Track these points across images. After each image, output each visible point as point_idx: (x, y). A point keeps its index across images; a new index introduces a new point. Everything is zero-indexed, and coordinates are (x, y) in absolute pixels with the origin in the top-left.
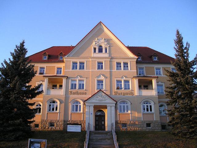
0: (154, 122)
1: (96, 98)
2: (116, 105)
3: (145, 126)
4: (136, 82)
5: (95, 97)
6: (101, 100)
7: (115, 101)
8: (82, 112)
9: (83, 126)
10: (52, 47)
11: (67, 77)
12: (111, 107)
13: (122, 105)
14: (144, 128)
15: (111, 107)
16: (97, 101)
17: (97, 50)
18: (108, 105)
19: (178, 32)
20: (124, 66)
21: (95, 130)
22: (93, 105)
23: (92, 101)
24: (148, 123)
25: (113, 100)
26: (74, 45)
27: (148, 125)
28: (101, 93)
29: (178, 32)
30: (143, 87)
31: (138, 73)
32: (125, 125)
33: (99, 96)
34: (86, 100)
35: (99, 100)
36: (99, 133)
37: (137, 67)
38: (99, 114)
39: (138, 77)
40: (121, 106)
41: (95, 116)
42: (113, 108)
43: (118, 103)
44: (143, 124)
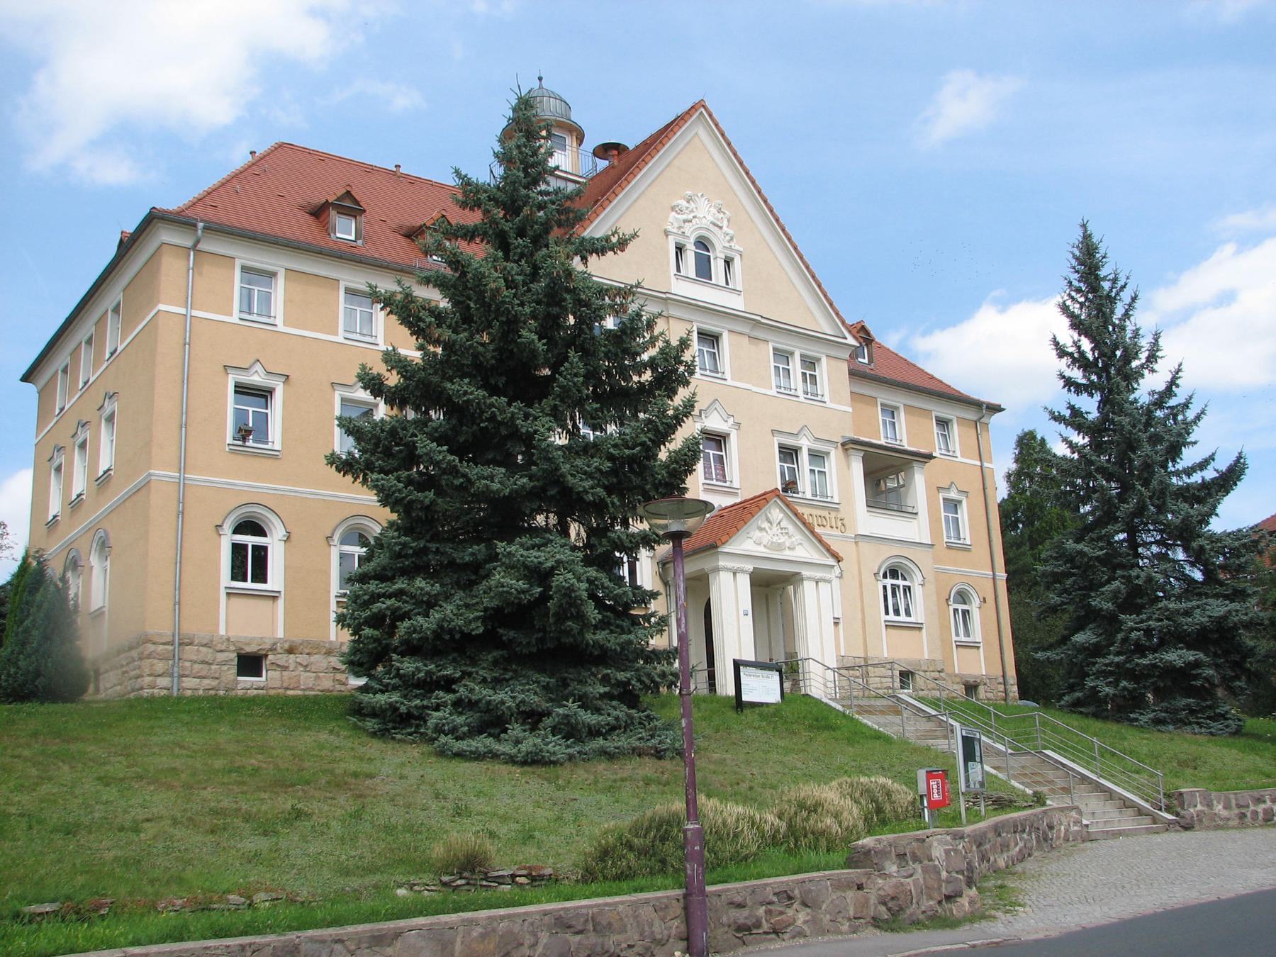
6: (779, 547)
16: (761, 551)
18: (806, 573)
25: (828, 549)
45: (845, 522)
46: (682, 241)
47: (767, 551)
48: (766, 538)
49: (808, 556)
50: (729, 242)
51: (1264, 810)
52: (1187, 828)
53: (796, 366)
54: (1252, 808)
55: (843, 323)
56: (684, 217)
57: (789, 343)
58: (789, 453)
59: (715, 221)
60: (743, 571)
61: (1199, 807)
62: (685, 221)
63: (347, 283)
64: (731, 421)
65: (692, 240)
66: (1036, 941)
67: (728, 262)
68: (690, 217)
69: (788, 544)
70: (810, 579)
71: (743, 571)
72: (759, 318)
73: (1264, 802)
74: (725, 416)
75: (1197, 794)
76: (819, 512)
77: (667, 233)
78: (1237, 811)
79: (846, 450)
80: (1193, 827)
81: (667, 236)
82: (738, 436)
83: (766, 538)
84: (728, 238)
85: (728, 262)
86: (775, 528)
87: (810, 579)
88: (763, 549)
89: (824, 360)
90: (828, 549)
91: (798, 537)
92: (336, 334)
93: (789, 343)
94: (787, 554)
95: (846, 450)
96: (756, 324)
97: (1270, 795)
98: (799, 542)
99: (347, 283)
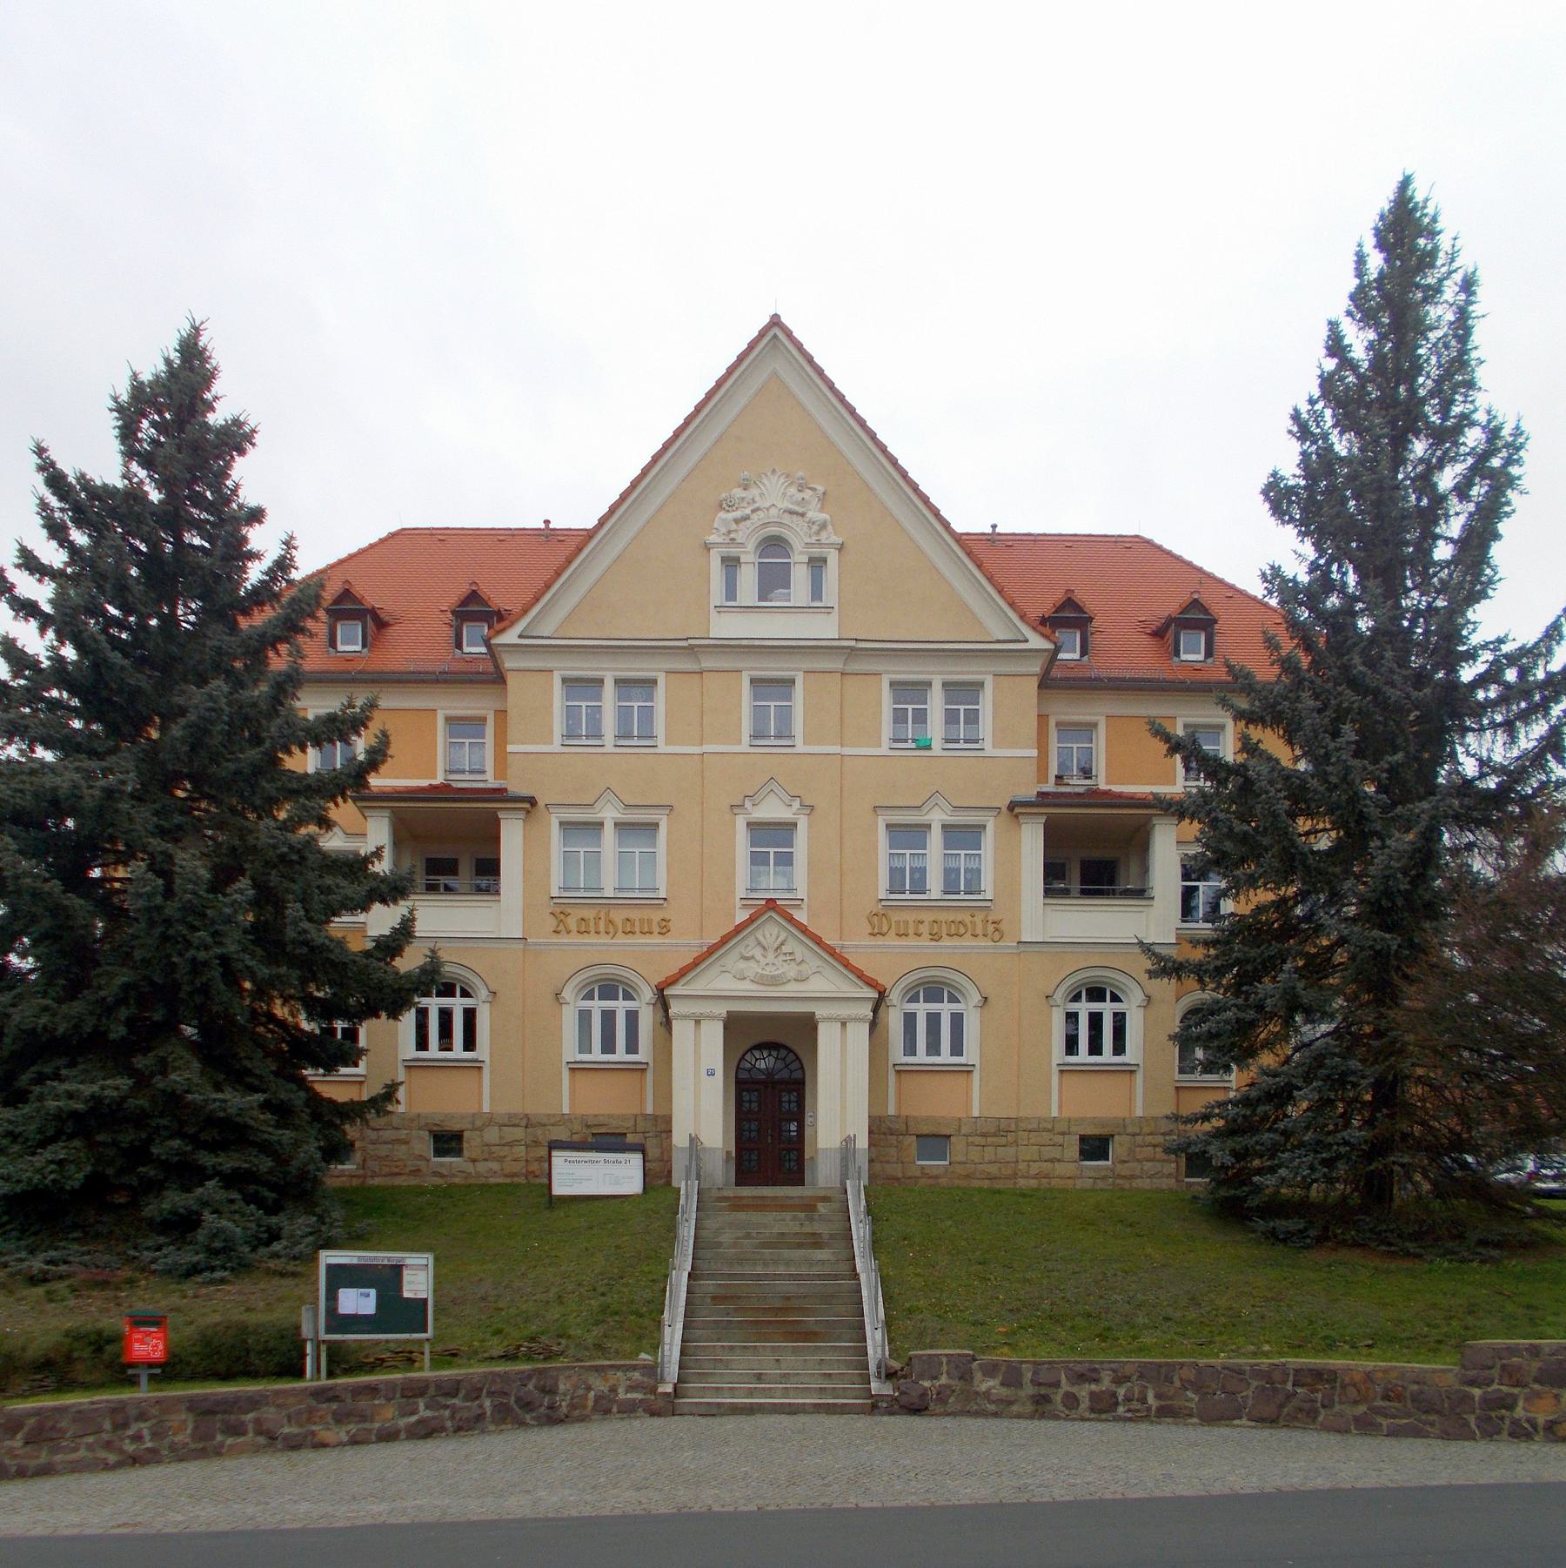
0: (1129, 1130)
1: (742, 965)
2: (875, 1011)
3: (1073, 1151)
4: (1031, 843)
5: (731, 960)
6: (775, 981)
7: (871, 983)
8: (643, 1055)
9: (653, 1152)
10: (393, 536)
11: (532, 801)
12: (844, 1024)
13: (922, 1009)
14: (1060, 1169)
15: (844, 1024)
16: (746, 987)
17: (748, 579)
18: (820, 1011)
19: (40, 451)
20: (951, 718)
21: (740, 1181)
22: (722, 1009)
23: (718, 986)
24: (1090, 1131)
25: (860, 975)
26: (580, 515)
27: (1095, 1147)
28: (771, 931)
29: (40, 451)
30: (1075, 873)
31: (1054, 771)
32: (934, 1141)
33: (758, 952)
34: (673, 981)
35: (760, 980)
36: (759, 1205)
37: (1042, 719)
38: (764, 1062)
39: (1044, 798)
40: (910, 1019)
41: (739, 1082)
42: (859, 1035)
43: (894, 996)
44: (1059, 1139)
45: (1002, 926)
46: (733, 551)
47: (762, 988)
48: (752, 969)
49: (833, 988)
50: (818, 533)
51: (1092, 1394)
52: (917, 1410)
53: (936, 704)
54: (1066, 1387)
55: (1022, 617)
56: (738, 514)
57: (974, 669)
58: (908, 835)
59: (791, 506)
60: (711, 1018)
61: (944, 1380)
62: (737, 521)
63: (752, 673)
64: (796, 804)
65: (751, 547)
66: (909, 1510)
67: (817, 564)
68: (748, 511)
69: (792, 974)
70: (829, 1019)
71: (711, 1018)
72: (853, 643)
73: (1097, 1381)
74: (787, 799)
75: (944, 1360)
76: (951, 916)
77: (707, 547)
78: (1029, 1390)
79: (1016, 816)
80: (926, 1408)
81: (709, 550)
82: (810, 826)
83: (752, 969)
84: (815, 528)
85: (817, 564)
86: (771, 956)
87: (829, 1019)
88: (754, 987)
89: (989, 682)
90: (860, 975)
91: (813, 963)
92: (739, 742)
93: (974, 669)
94: (791, 989)
95: (1016, 816)
96: (852, 653)
97: (1114, 1371)
98: (814, 970)
99: (752, 673)
